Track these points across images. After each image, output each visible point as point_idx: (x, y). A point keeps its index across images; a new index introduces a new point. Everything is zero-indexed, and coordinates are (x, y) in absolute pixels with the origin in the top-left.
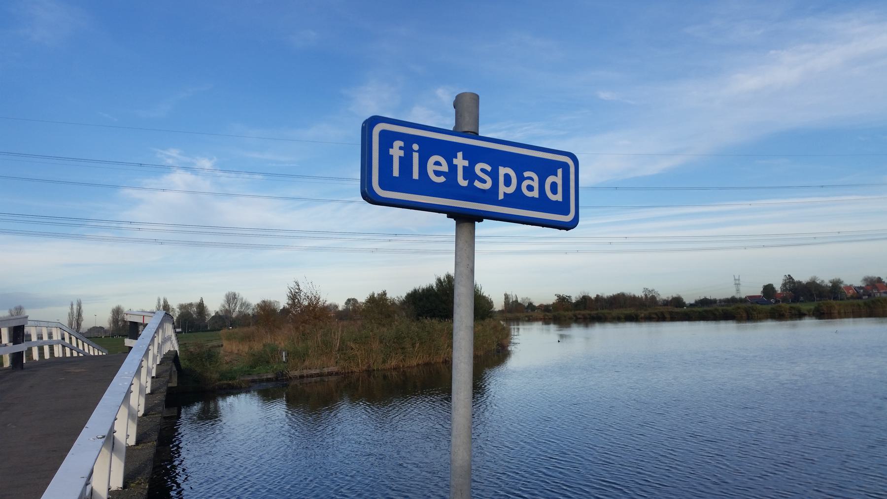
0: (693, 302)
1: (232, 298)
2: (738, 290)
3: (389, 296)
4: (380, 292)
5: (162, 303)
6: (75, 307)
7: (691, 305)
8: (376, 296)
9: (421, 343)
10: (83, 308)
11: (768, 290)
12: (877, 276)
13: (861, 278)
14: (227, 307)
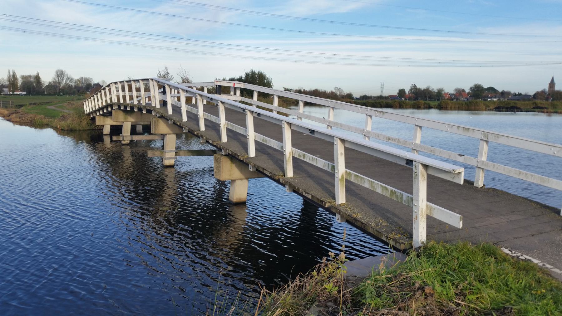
0: (358, 97)
1: (60, 74)
2: (382, 92)
5: (11, 74)
7: (357, 99)
11: (402, 92)
12: (462, 88)
13: (454, 88)
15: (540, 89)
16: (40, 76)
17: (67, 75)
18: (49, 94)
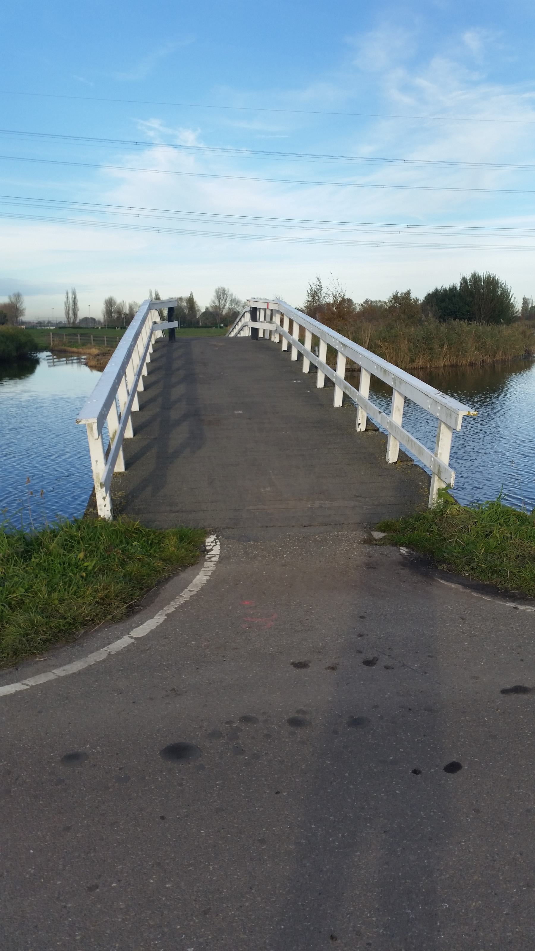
1: (221, 294)
3: (413, 296)
4: (404, 291)
5: (154, 296)
6: (70, 295)
8: (399, 295)
9: (450, 345)
10: (78, 297)
14: (217, 302)
15: (447, 286)
16: (195, 298)
17: (232, 295)
18: (205, 326)
